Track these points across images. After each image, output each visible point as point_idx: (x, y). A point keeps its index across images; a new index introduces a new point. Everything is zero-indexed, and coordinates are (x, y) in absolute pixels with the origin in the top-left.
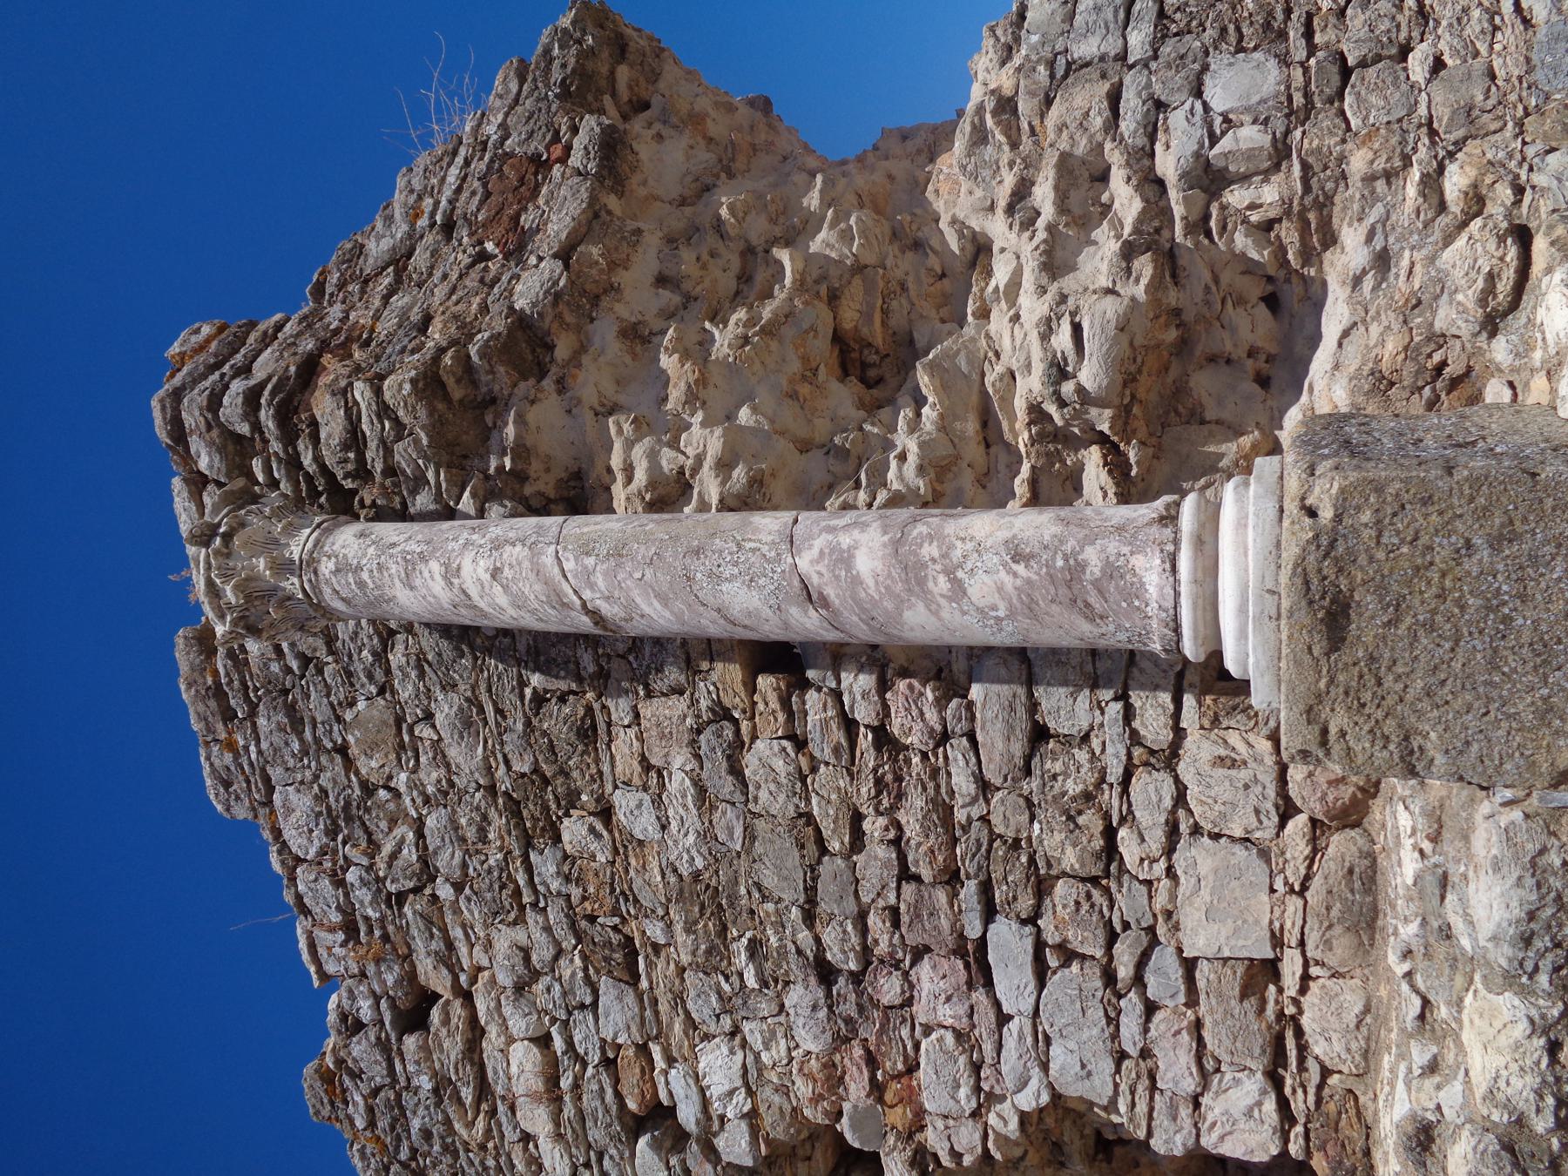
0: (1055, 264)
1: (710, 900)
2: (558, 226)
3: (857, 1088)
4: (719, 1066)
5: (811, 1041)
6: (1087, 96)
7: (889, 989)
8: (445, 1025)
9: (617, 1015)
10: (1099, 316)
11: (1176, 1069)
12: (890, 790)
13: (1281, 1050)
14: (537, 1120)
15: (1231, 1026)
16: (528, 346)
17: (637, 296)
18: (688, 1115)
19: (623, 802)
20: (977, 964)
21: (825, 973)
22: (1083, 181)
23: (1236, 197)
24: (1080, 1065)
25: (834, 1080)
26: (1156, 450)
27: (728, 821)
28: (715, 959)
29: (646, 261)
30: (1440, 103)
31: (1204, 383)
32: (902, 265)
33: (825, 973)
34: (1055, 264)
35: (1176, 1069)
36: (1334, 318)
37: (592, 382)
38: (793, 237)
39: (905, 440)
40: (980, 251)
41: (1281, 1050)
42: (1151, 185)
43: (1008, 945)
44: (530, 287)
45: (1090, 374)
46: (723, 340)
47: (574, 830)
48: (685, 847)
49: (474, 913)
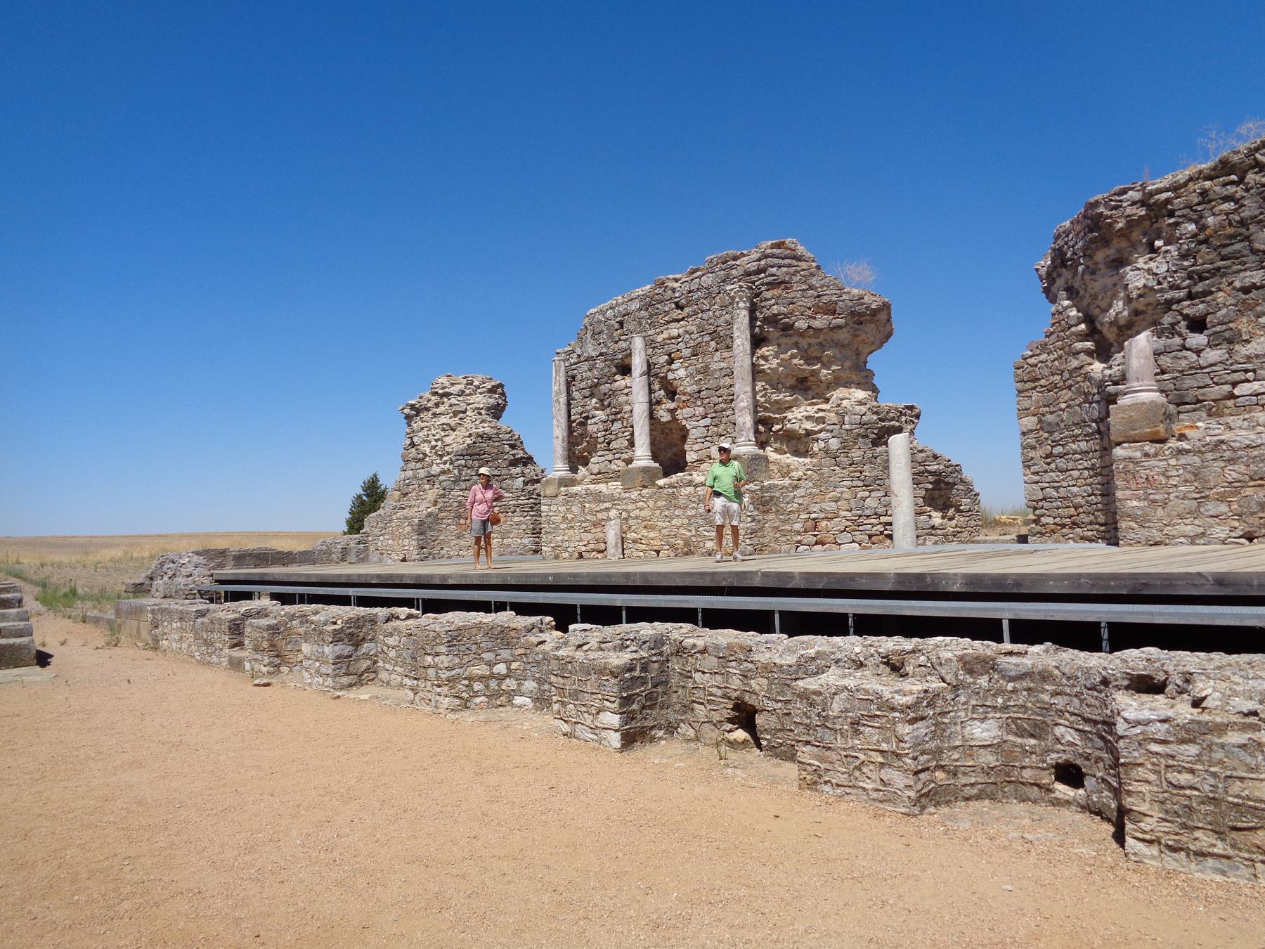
0: (808, 418)
1: (706, 371)
2: (817, 324)
3: (684, 398)
4: (682, 373)
5: (689, 390)
6: (835, 420)
7: (699, 403)
8: (676, 314)
9: (686, 352)
10: (796, 427)
11: (696, 447)
12: (725, 402)
13: (701, 461)
14: (665, 335)
15: (703, 454)
16: (788, 328)
17: (804, 343)
18: (673, 366)
19: (718, 354)
20: (704, 417)
21: (699, 392)
22: (821, 420)
23: (1119, 452)
24: (694, 434)
25: (684, 394)
26: (783, 436)
27: (717, 374)
28: (698, 372)
29: (813, 341)
30: (825, 470)
31: (794, 442)
32: (824, 386)
33: (699, 392)
34: (808, 418)
35: (696, 447)
36: (801, 460)
37: (784, 340)
38: (825, 366)
39: (781, 396)
40: (827, 400)
41: (701, 461)
42: (820, 431)
43: (707, 421)
44: (801, 324)
45: (789, 426)
46: (795, 361)
47: (713, 344)
48: (714, 366)
49: (697, 322)
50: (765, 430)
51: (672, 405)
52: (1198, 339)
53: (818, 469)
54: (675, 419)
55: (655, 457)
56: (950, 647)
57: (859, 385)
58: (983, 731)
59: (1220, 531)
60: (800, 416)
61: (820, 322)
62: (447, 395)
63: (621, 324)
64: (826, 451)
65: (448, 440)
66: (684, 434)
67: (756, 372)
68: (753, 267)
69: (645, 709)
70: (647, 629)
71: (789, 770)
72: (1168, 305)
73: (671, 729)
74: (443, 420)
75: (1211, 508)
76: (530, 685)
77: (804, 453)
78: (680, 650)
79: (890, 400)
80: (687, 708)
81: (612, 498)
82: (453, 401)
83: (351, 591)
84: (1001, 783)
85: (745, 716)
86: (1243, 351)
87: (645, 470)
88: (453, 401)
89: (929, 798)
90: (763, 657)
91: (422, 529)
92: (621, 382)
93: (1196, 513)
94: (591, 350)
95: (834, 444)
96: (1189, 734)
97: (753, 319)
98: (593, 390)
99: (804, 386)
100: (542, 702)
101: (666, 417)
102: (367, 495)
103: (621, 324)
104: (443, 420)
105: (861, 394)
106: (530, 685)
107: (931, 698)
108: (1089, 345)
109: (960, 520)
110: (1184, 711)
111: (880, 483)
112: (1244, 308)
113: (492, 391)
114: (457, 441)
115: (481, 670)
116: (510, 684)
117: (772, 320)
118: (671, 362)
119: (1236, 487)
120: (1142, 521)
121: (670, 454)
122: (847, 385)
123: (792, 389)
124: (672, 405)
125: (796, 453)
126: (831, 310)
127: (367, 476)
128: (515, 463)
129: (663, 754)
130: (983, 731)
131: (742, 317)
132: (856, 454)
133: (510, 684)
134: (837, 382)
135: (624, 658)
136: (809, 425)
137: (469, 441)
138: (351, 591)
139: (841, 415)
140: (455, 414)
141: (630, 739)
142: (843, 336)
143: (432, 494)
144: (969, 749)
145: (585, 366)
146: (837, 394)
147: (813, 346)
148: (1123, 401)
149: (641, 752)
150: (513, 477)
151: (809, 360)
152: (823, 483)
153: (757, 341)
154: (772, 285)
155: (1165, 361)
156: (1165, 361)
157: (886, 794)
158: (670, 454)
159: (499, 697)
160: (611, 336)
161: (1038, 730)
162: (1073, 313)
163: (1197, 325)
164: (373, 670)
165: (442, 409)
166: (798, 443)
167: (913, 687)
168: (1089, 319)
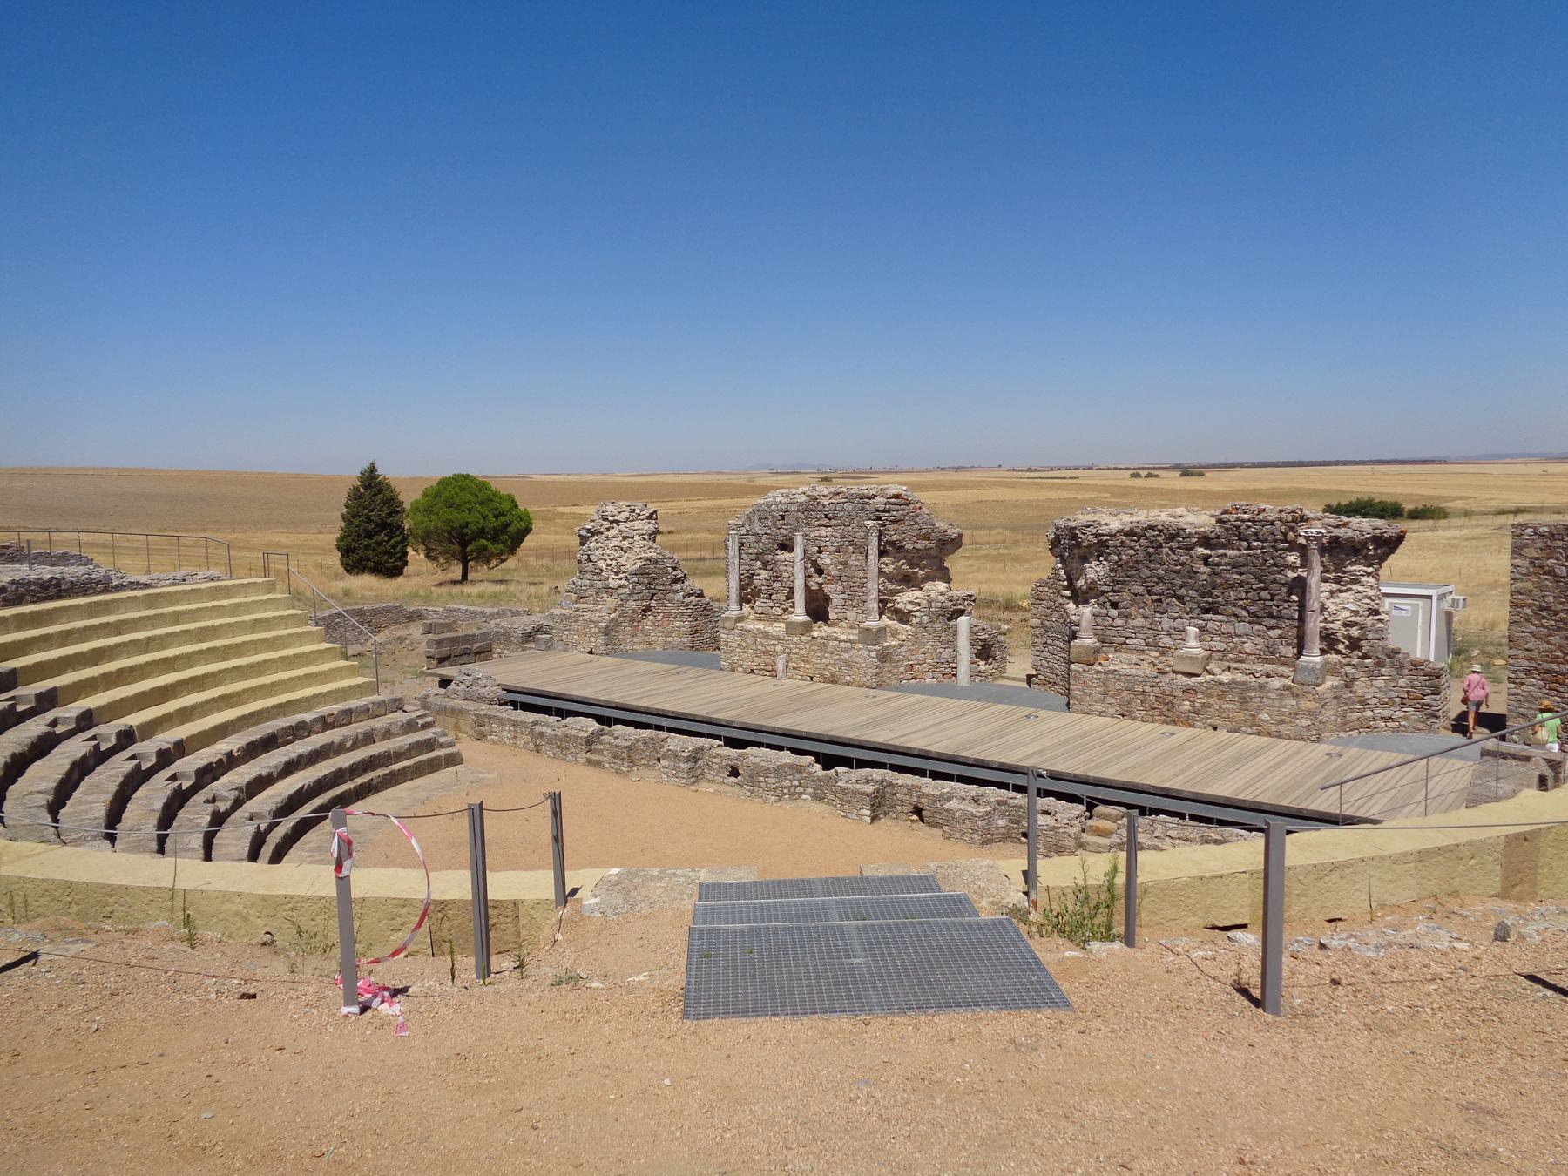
1: (845, 563)
4: (828, 561)
9: (832, 549)
23: (1073, 667)
44: (909, 546)
50: (884, 606)
51: (820, 580)
52: (1114, 612)
53: (915, 634)
54: (821, 589)
55: (808, 614)
56: (992, 793)
57: (940, 579)
58: (1001, 822)
59: (1111, 711)
60: (905, 599)
61: (921, 545)
62: (617, 522)
63: (783, 518)
64: (920, 624)
65: (622, 561)
66: (827, 599)
67: (881, 572)
68: (881, 507)
69: (879, 805)
70: (877, 774)
71: (938, 832)
72: (1103, 592)
73: (886, 814)
74: (615, 542)
75: (1109, 700)
76: (810, 790)
77: (907, 622)
78: (891, 785)
79: (959, 591)
80: (893, 806)
81: (778, 638)
82: (622, 527)
83: (665, 722)
84: (1006, 838)
85: (918, 811)
86: (1132, 623)
87: (804, 624)
88: (622, 527)
89: (986, 842)
90: (926, 790)
91: (607, 631)
92: (783, 556)
93: (1102, 701)
94: (757, 528)
95: (925, 620)
96: (1053, 829)
97: (880, 540)
98: (759, 556)
99: (908, 581)
100: (816, 797)
101: (815, 587)
102: (366, 488)
103: (783, 518)
104: (615, 542)
105: (941, 586)
106: (810, 790)
107: (987, 813)
108: (1067, 593)
109: (995, 664)
110: (1053, 823)
111: (951, 644)
112: (1134, 603)
113: (650, 517)
114: (630, 562)
115: (787, 783)
116: (800, 789)
117: (892, 543)
118: (820, 552)
119: (1119, 692)
120: (1080, 701)
121: (818, 609)
122: (933, 579)
123: (901, 582)
124: (820, 580)
125: (901, 621)
126: (927, 537)
127: (365, 465)
128: (676, 581)
129: (885, 823)
130: (1001, 822)
131: (874, 542)
132: (938, 626)
133: (800, 789)
134: (928, 578)
135: (870, 789)
136: (910, 607)
137: (640, 563)
138: (665, 722)
139: (930, 602)
140: (625, 538)
141: (874, 818)
142: (933, 553)
143: (611, 602)
144: (997, 828)
145: (753, 539)
146: (927, 586)
147: (915, 559)
148: (1078, 641)
149: (877, 823)
150: (675, 592)
151: (912, 565)
152: (917, 642)
153: (882, 553)
154: (893, 522)
155: (1099, 620)
156: (1099, 620)
157: (973, 842)
158: (818, 609)
159: (796, 796)
160: (774, 523)
161: (1017, 822)
162: (1062, 573)
163: (1114, 605)
164: (702, 774)
165: (611, 533)
166: (903, 617)
167: (982, 810)
168: (1069, 579)
